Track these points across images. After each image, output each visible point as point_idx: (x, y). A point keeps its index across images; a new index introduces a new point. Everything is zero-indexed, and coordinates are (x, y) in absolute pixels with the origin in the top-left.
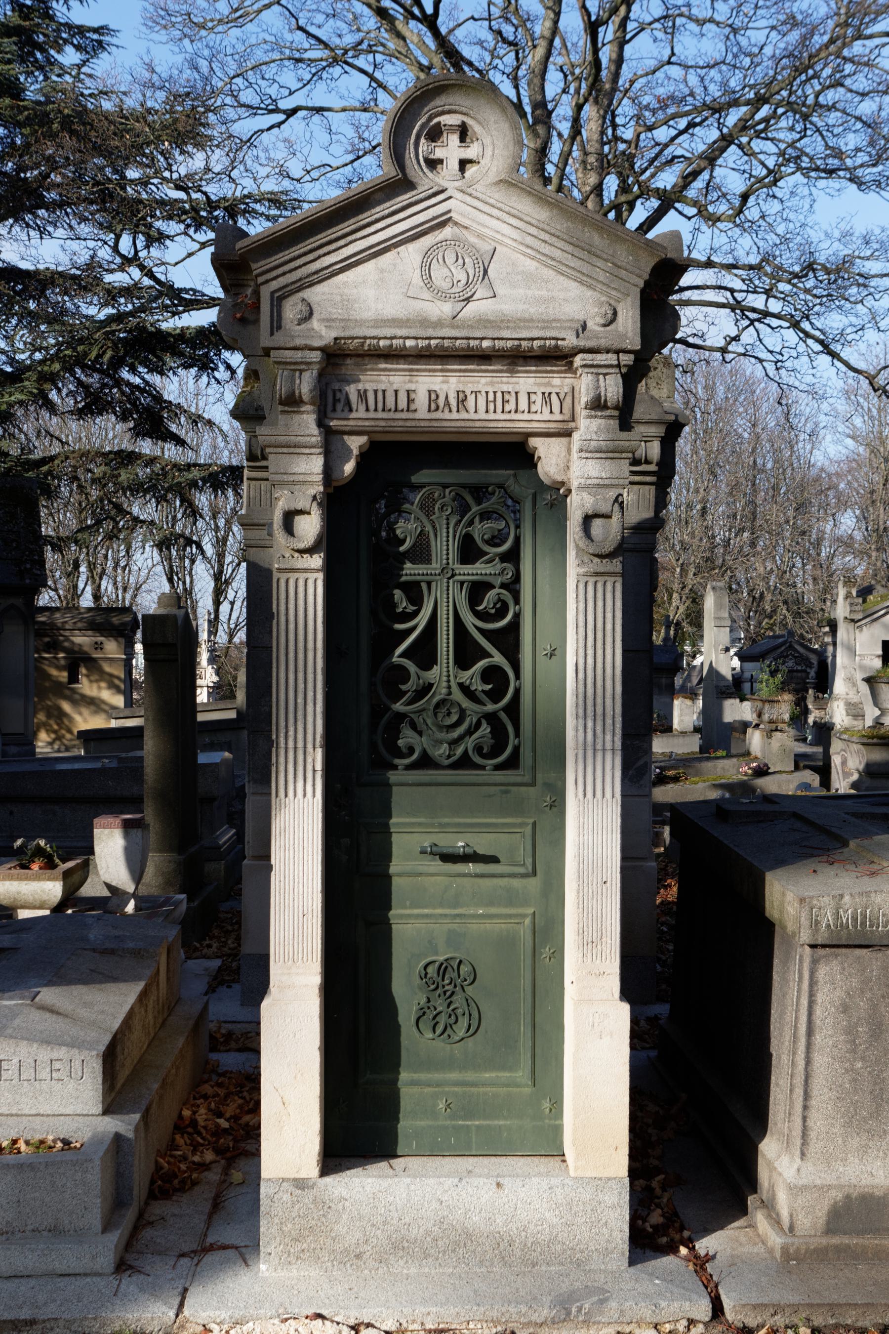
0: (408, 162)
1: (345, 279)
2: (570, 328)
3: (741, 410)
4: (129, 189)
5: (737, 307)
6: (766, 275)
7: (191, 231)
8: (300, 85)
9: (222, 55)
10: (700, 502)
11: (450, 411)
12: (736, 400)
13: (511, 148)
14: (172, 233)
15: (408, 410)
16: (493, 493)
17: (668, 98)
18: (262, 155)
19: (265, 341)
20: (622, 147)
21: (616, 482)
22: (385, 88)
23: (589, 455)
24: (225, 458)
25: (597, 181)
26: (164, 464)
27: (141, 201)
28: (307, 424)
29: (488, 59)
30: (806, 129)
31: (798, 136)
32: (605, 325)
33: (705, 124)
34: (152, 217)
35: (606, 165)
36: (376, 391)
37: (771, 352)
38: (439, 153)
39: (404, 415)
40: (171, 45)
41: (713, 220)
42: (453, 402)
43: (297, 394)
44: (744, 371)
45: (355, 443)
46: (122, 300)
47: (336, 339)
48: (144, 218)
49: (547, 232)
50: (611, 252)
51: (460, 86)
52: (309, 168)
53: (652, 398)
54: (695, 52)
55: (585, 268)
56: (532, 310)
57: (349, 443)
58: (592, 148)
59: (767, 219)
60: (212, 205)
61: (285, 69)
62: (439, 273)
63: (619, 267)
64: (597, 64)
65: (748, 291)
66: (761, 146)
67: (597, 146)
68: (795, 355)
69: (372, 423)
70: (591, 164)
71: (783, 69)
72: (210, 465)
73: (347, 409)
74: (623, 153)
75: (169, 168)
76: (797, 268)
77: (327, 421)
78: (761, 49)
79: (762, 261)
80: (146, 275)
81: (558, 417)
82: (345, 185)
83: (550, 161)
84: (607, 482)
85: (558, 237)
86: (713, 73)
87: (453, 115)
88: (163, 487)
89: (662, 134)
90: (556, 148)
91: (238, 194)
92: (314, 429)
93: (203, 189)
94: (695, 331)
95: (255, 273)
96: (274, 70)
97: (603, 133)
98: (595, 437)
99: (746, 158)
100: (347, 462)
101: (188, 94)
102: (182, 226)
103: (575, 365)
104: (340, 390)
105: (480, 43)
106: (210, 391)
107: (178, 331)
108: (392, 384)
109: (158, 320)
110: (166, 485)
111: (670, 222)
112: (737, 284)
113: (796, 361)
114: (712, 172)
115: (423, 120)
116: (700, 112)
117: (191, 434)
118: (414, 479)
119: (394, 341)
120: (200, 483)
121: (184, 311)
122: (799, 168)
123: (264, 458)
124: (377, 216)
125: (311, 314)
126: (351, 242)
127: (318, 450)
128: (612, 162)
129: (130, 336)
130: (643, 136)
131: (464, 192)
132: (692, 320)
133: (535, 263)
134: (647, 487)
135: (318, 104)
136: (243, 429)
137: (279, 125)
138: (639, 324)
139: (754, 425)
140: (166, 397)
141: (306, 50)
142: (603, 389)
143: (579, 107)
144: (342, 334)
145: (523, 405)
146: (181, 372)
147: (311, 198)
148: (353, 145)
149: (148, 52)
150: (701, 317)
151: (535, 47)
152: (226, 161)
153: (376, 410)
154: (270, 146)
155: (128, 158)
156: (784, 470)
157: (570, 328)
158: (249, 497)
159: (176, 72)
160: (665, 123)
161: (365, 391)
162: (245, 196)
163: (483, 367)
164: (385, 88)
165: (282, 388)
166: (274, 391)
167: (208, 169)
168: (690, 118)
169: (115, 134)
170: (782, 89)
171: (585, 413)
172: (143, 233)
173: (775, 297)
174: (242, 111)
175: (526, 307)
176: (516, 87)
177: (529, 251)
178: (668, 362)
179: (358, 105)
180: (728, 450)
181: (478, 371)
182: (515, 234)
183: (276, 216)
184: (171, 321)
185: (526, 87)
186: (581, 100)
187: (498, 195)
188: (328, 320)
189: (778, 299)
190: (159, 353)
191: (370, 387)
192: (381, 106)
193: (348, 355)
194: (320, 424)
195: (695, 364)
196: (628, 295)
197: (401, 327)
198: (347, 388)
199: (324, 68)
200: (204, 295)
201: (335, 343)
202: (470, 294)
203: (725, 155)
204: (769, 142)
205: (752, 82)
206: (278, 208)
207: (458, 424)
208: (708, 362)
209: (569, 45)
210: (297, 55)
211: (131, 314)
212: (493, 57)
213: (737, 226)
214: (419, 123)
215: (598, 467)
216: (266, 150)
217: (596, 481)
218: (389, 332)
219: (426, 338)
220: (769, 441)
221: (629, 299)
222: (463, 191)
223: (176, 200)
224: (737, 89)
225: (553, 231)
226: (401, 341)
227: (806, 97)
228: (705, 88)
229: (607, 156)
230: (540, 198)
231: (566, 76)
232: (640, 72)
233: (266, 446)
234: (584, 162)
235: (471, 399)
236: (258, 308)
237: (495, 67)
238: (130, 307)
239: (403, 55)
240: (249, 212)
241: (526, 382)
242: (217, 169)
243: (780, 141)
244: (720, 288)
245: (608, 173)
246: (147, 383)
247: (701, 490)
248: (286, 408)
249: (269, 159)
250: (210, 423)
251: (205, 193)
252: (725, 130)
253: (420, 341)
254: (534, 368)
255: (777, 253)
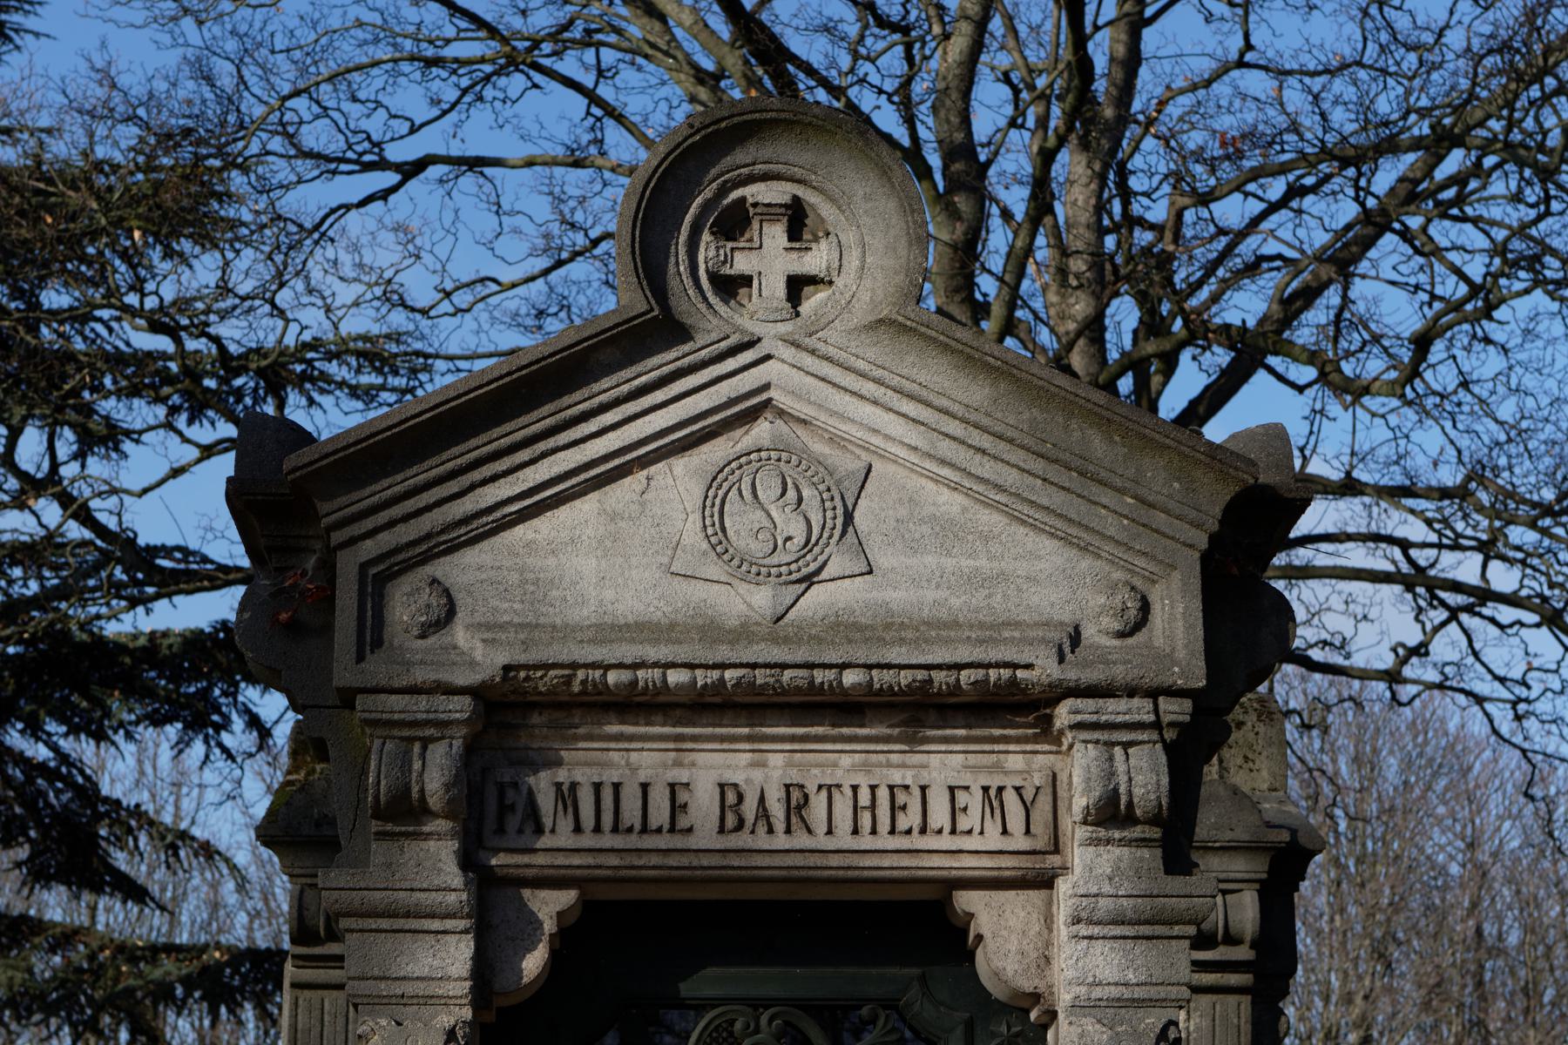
0: (673, 283)
1: (530, 535)
2: (1043, 641)
3: (1441, 810)
4: (45, 331)
5: (1416, 580)
6: (1480, 509)
7: (181, 421)
8: (436, 112)
9: (264, 52)
10: (1357, 1026)
11: (771, 831)
12: (1429, 788)
13: (903, 252)
14: (138, 426)
15: (672, 830)
16: (873, 1021)
17: (1244, 136)
18: (346, 259)
19: (345, 673)
20: (1143, 237)
21: (1162, 992)
22: (620, 119)
23: (1096, 930)
24: (239, 931)
25: (1090, 311)
26: (95, 945)
27: (69, 356)
28: (437, 863)
29: (845, 61)
30: (1548, 199)
31: (1533, 213)
32: (1121, 635)
33: (1326, 188)
34: (93, 390)
35: (1109, 277)
36: (597, 787)
37: (1502, 680)
38: (742, 264)
39: (663, 842)
40: (152, 32)
41: (1355, 391)
42: (777, 810)
43: (415, 794)
44: (1443, 721)
45: (549, 906)
46: (17, 572)
47: (507, 668)
48: (75, 393)
49: (985, 430)
50: (1131, 472)
51: (789, 124)
52: (449, 286)
53: (1235, 791)
54: (1298, 42)
55: (1076, 508)
56: (956, 602)
57: (534, 906)
58: (1078, 240)
59: (1476, 389)
60: (229, 364)
61: (402, 80)
62: (742, 523)
63: (1151, 506)
64: (1083, 67)
65: (1440, 546)
66: (1453, 235)
67: (1090, 236)
68: (1557, 686)
69: (589, 860)
70: (1077, 276)
71: (1490, 75)
72: (205, 948)
73: (529, 830)
74: (1147, 251)
75: (138, 287)
76: (1549, 495)
77: (482, 854)
78: (1440, 35)
79: (1468, 479)
80: (75, 516)
81: (1022, 843)
82: (530, 322)
83: (985, 270)
84: (1139, 993)
85: (1011, 441)
86: (1339, 85)
87: (774, 184)
88: (90, 999)
89: (1232, 211)
90: (998, 240)
91: (290, 340)
92: (452, 875)
93: (212, 330)
94: (1325, 636)
95: (325, 522)
96: (379, 83)
97: (1101, 208)
98: (1107, 889)
99: (1421, 260)
100: (529, 950)
101: (187, 132)
102: (161, 411)
103: (1058, 724)
104: (515, 785)
105: (828, 29)
106: (209, 776)
107: (142, 641)
108: (634, 770)
109: (98, 617)
110: (99, 994)
111: (1261, 404)
112: (1415, 531)
113: (1559, 701)
114: (1346, 289)
115: (708, 193)
116: (1314, 166)
117: (161, 873)
118: (686, 989)
119: (641, 674)
120: (179, 991)
121: (157, 597)
122: (1538, 282)
123: (333, 936)
124: (603, 398)
125: (451, 612)
126: (544, 455)
127: (462, 924)
128: (1123, 272)
129: (32, 652)
130: (1189, 216)
131: (798, 346)
132: (1320, 610)
133: (959, 499)
134: (1232, 999)
135: (472, 152)
136: (285, 868)
137: (384, 195)
138: (1199, 631)
139: (1471, 846)
140: (105, 790)
141: (448, 41)
142: (1123, 779)
143: (1046, 157)
144: (523, 658)
145: (939, 815)
146: (147, 733)
147: (453, 349)
148: (547, 236)
149: (103, 45)
150: (1337, 603)
151: (946, 37)
152: (266, 271)
153: (597, 829)
154: (364, 240)
155: (46, 265)
156: (1549, 948)
157: (1043, 641)
158: (294, 1028)
159: (164, 86)
160: (1238, 189)
161: (574, 786)
162: (306, 346)
163: (845, 730)
164: (620, 119)
165: (379, 778)
166: (361, 787)
167: (224, 289)
168: (1291, 177)
169: (21, 213)
170: (1489, 117)
171: (1082, 833)
172: (72, 426)
173: (1504, 558)
174: (305, 167)
175: (941, 594)
176: (910, 121)
177: (945, 472)
178: (1271, 713)
179: (560, 151)
180: (1415, 902)
181: (834, 740)
182: (914, 436)
183: (372, 386)
184: (127, 618)
185: (930, 121)
186: (1052, 141)
187: (869, 353)
188: (489, 627)
189: (1510, 561)
190: (96, 690)
191: (580, 775)
192: (614, 156)
193: (533, 706)
194: (467, 862)
195: (1328, 708)
196: (1173, 567)
197: (656, 642)
198: (531, 780)
199: (487, 79)
200: (205, 559)
201: (505, 678)
202: (813, 567)
203: (1372, 253)
204: (1468, 227)
205: (1424, 102)
206: (380, 371)
207: (789, 860)
208: (1359, 705)
209: (1023, 30)
210: (430, 52)
211: (34, 602)
212: (856, 56)
213: (1410, 403)
214: (699, 201)
215: (1116, 958)
216: (355, 248)
217: (1114, 992)
218: (629, 652)
219: (715, 666)
220: (1509, 881)
221: (1176, 575)
222: (796, 345)
223: (149, 354)
224: (1395, 116)
225: (998, 428)
226: (657, 673)
227: (1545, 133)
228: (1323, 115)
229: (1112, 257)
230: (969, 357)
231: (1016, 91)
232: (1179, 83)
233: (339, 915)
234: (1062, 272)
235: (819, 804)
236: (331, 600)
237: (862, 81)
238: (34, 586)
239: (664, 50)
240: (313, 380)
241: (945, 763)
242: (245, 288)
243: (1493, 223)
244: (1377, 538)
245: (1117, 294)
246: (63, 757)
247: (1359, 1000)
248: (389, 827)
249: (361, 266)
250: (207, 851)
251: (216, 340)
252: (1371, 203)
253: (698, 672)
254: (962, 732)
255: (1503, 461)
